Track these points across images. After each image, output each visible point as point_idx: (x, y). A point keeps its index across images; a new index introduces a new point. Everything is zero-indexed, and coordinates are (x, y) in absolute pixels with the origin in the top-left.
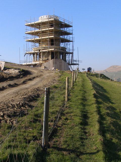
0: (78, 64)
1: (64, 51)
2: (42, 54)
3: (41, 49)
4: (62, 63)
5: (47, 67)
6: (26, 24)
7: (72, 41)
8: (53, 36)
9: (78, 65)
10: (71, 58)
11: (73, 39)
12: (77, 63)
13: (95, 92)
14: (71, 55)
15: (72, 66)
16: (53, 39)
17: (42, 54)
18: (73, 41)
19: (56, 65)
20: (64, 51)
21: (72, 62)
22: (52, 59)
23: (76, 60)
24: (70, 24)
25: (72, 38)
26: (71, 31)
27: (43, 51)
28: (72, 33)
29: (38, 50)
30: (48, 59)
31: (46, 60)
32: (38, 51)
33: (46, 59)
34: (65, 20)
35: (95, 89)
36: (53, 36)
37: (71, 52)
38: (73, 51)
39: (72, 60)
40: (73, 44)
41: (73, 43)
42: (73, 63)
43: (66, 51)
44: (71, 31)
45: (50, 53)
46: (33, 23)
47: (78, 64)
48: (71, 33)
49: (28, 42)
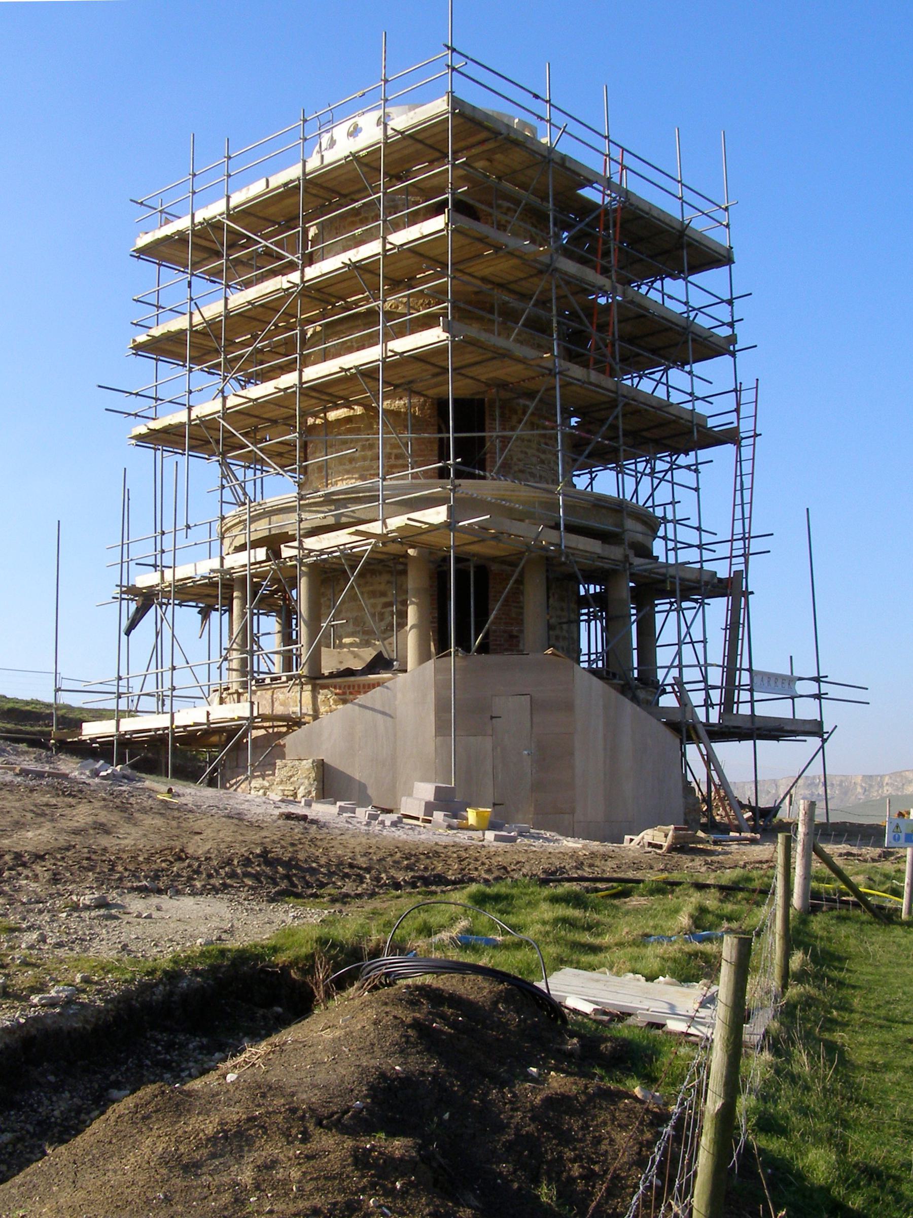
0: (815, 729)
1: (616, 552)
2: (303, 583)
3: (288, 523)
4: (568, 707)
5: (357, 771)
6: (143, 240)
7: (731, 437)
8: (434, 336)
9: (815, 742)
10: (716, 652)
11: (745, 411)
12: (807, 710)
13: (84, 738)
14: (718, 608)
15: (721, 749)
16: (483, 431)
17: (303, 583)
18: (746, 427)
19: (487, 743)
20: (616, 552)
21: (728, 703)
22: (424, 657)
23: (791, 680)
24: (689, 213)
25: (729, 402)
26: (723, 312)
27: (311, 543)
28: (732, 339)
29: (255, 544)
30: (380, 663)
31: (349, 672)
32: (261, 554)
33: (368, 654)
34: (629, 161)
35: (341, 551)
36: (434, 336)
37: (722, 571)
38: (746, 556)
39: (731, 668)
40: (747, 467)
41: (746, 452)
42: (745, 709)
43: (646, 552)
44: (723, 312)
45: (414, 580)
46: (215, 210)
47: (815, 729)
48: (725, 332)
49: (171, 460)
